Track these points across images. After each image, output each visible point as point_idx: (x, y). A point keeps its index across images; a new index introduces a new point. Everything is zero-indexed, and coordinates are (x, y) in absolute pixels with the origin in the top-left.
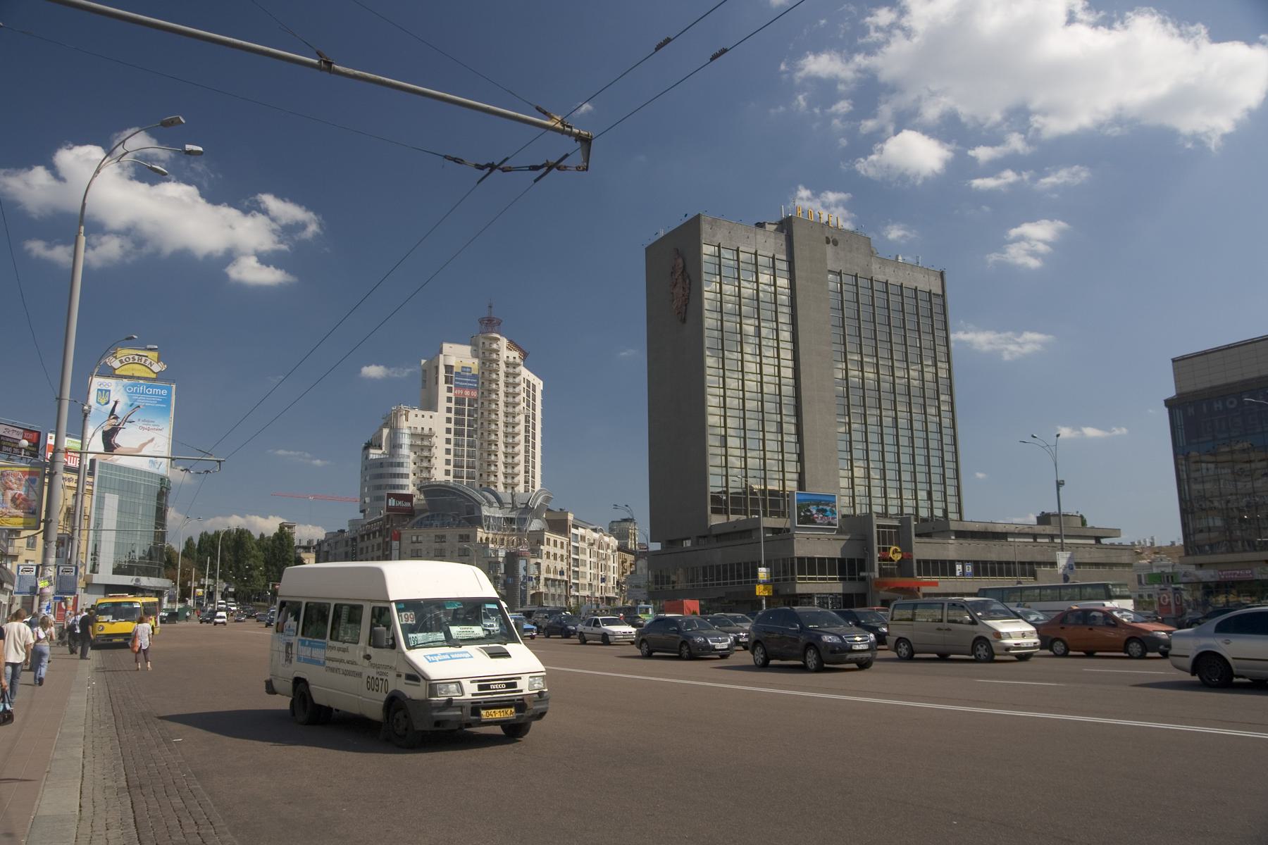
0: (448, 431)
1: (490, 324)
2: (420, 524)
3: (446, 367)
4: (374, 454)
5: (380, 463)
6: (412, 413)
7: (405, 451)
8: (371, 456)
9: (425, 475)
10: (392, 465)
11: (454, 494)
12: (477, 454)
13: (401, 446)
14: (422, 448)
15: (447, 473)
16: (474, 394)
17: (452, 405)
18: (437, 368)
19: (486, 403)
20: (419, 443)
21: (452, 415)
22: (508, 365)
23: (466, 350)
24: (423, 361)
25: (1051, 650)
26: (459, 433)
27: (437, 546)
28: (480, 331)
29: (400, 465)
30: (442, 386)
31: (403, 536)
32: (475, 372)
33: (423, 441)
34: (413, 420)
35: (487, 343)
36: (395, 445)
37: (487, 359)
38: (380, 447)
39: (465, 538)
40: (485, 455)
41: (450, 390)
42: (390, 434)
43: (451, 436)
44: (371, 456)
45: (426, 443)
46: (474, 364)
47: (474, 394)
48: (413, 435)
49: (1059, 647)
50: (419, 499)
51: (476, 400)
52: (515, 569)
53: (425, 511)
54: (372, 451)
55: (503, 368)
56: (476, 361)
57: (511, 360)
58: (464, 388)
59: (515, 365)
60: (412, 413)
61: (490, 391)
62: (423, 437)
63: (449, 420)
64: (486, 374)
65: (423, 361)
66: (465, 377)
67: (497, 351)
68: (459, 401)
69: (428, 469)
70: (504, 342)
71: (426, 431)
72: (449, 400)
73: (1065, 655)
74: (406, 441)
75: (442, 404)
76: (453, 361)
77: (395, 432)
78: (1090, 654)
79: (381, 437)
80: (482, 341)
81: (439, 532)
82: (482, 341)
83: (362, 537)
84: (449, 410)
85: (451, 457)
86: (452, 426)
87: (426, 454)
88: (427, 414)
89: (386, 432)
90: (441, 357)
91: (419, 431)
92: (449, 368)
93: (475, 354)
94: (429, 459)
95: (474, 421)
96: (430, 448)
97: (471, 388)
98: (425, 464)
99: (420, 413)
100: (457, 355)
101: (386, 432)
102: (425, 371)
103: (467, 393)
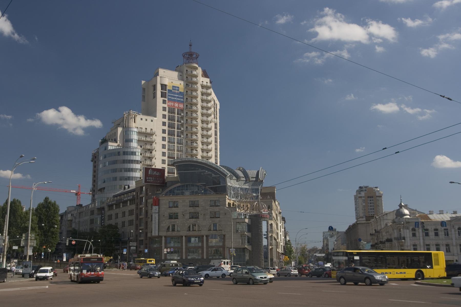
0: (164, 131)
1: (190, 57)
2: (172, 192)
3: (162, 85)
4: (112, 146)
5: (116, 153)
6: (138, 117)
7: (134, 144)
8: (110, 148)
9: (148, 162)
10: (125, 153)
11: (203, 168)
12: (184, 149)
13: (131, 141)
14: (146, 143)
15: (164, 162)
16: (181, 106)
17: (166, 113)
18: (155, 87)
19: (189, 113)
20: (143, 139)
21: (166, 120)
22: (203, 87)
23: (175, 74)
24: (143, 82)
25: (365, 282)
26: (171, 134)
27: (192, 210)
28: (185, 61)
29: (134, 153)
30: (159, 99)
31: (162, 202)
32: (181, 90)
33: (146, 138)
34: (140, 123)
35: (189, 70)
36: (127, 140)
37: (190, 83)
38: (116, 141)
39: (215, 204)
40: (189, 150)
41: (164, 102)
42: (123, 132)
43: (166, 135)
44: (110, 148)
45: (148, 139)
46: (180, 84)
47: (181, 106)
48: (139, 133)
49: (342, 280)
50: (172, 174)
51: (182, 110)
52: (259, 228)
53: (176, 182)
54: (110, 144)
55: (200, 89)
56: (182, 83)
57: (205, 83)
58: (174, 101)
59: (208, 88)
60: (138, 117)
61: (192, 104)
62: (146, 135)
63: (164, 124)
64: (189, 92)
65: (143, 82)
66: (175, 93)
67: (196, 76)
68: (171, 111)
69: (150, 158)
70: (199, 71)
71: (149, 131)
72: (164, 109)
73: (345, 284)
74: (135, 137)
75: (160, 112)
76: (166, 82)
77: (127, 130)
78: (356, 284)
79: (116, 133)
80: (185, 69)
81: (193, 198)
82: (185, 69)
83: (110, 207)
84: (164, 116)
85: (166, 150)
86: (166, 128)
87: (148, 147)
88: (150, 118)
89: (120, 130)
90: (158, 78)
91: (144, 130)
92: (164, 87)
93: (181, 78)
94: (151, 151)
95: (181, 125)
96: (151, 143)
97: (179, 102)
98: (148, 155)
99: (144, 117)
100: (169, 78)
101: (120, 130)
102: (144, 89)
103: (176, 105)
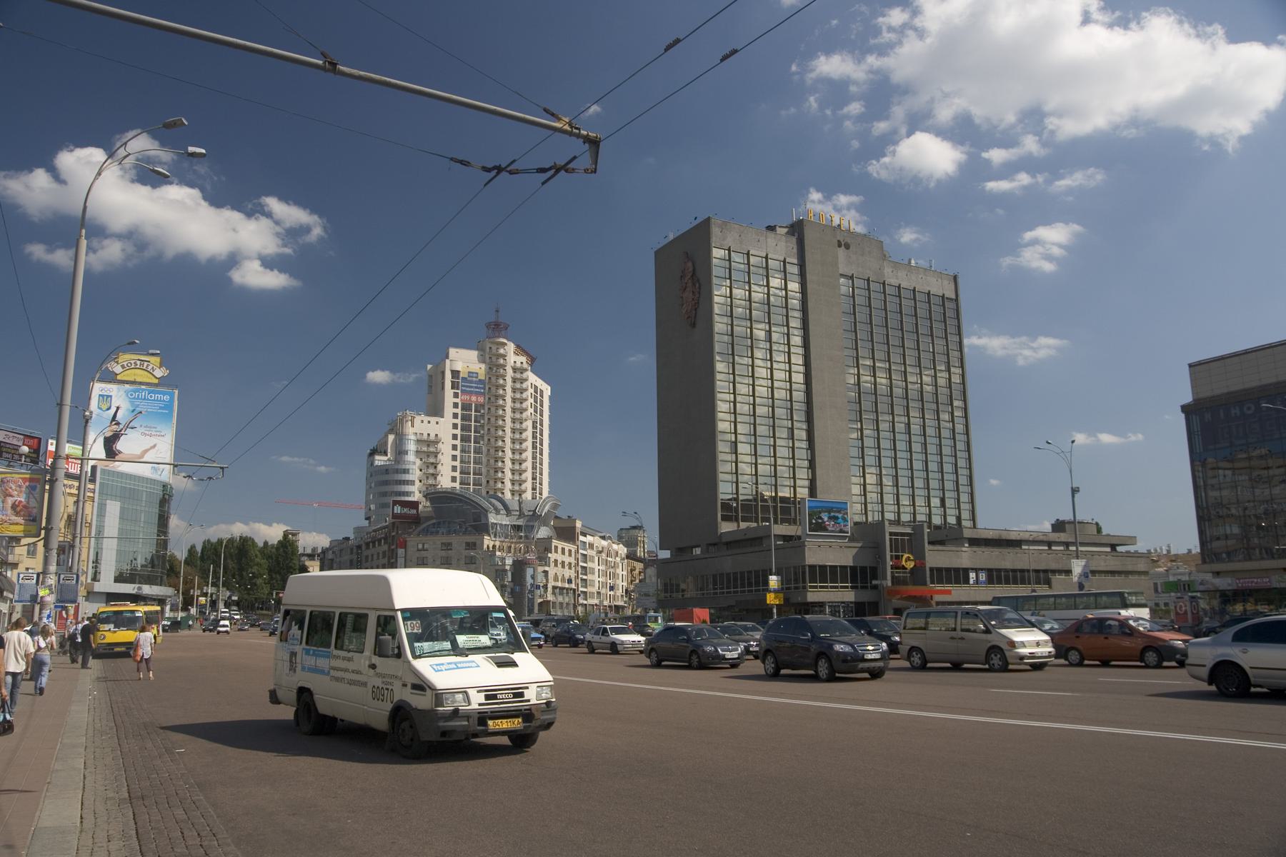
0: (455, 437)
1: (497, 328)
2: (426, 532)
3: (453, 372)
4: (380, 460)
5: (386, 470)
6: (418, 419)
7: (411, 457)
8: (377, 463)
9: (431, 481)
10: (397, 471)
11: (461, 501)
12: (484, 460)
13: (406, 453)
14: (428, 454)
15: (454, 479)
16: (481, 400)
17: (459, 411)
18: (443, 373)
19: (493, 409)
20: (425, 449)
21: (458, 421)
22: (515, 370)
23: (473, 355)
24: (429, 367)
25: (1066, 659)
26: (465, 439)
27: (443, 553)
28: (486, 335)
29: (406, 471)
30: (449, 392)
31: (409, 544)
32: (482, 377)
33: (429, 447)
34: (419, 426)
35: (494, 348)
36: (400, 452)
37: (494, 364)
38: (385, 454)
39: (472, 546)
40: (492, 461)
41: (456, 395)
42: (395, 440)
43: (458, 442)
44: (377, 463)
45: (432, 449)
46: (480, 369)
47: (481, 400)
48: (419, 441)
49: (1074, 656)
50: (425, 506)
51: (483, 406)
52: (523, 577)
53: (431, 518)
54: (377, 457)
55: (510, 373)
56: (483, 366)
57: (518, 365)
58: (470, 393)
59: (523, 371)
60: (418, 419)
61: (497, 397)
62: (429, 443)
63: (455, 426)
64: (493, 379)
65: (429, 367)
66: (471, 382)
67: (504, 356)
68: (466, 407)
69: (435, 476)
70: (511, 347)
71: (432, 437)
72: (456, 405)
73: (1080, 664)
74: (411, 447)
75: (449, 410)
76: (459, 366)
77: (401, 438)
78: (1105, 664)
79: (386, 443)
80: (488, 345)
81: (446, 539)
82: (488, 345)
83: (367, 544)
84: (455, 416)
85: (457, 463)
86: (458, 432)
87: (432, 460)
88: (433, 420)
89: (391, 438)
90: (448, 362)
91: (425, 437)
92: (455, 374)
93: (482, 359)
94: (435, 466)
95: (480, 427)
96: (436, 455)
97: (477, 394)
98: (431, 471)
99: (426, 419)
100: (464, 360)
101: (391, 438)
102: (431, 376)
103: (474, 398)
